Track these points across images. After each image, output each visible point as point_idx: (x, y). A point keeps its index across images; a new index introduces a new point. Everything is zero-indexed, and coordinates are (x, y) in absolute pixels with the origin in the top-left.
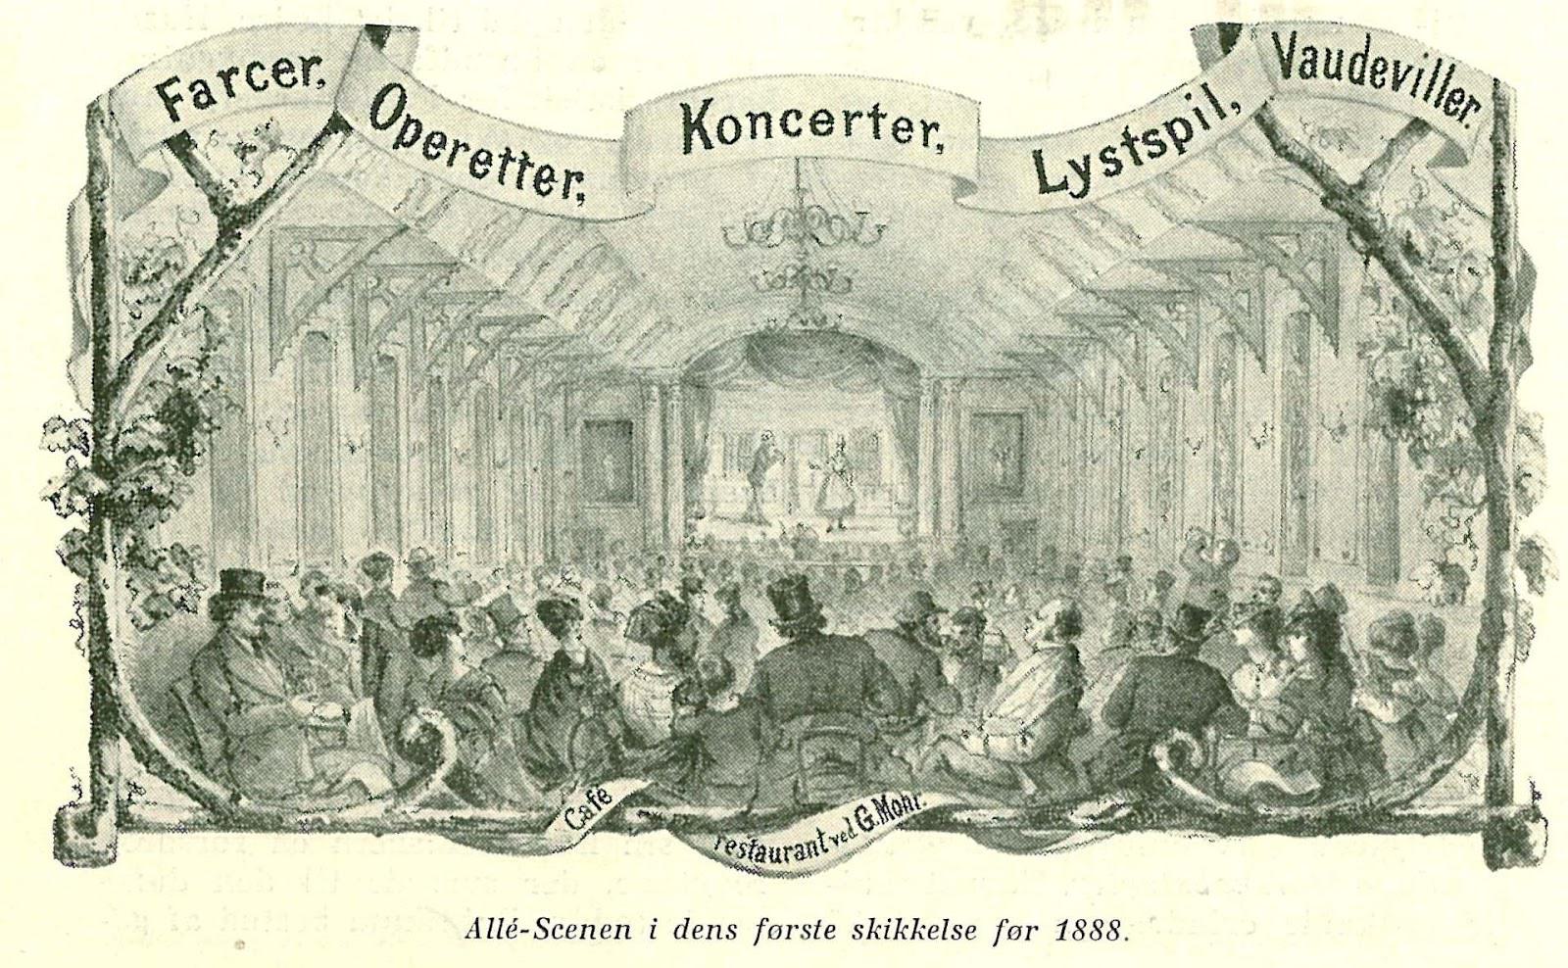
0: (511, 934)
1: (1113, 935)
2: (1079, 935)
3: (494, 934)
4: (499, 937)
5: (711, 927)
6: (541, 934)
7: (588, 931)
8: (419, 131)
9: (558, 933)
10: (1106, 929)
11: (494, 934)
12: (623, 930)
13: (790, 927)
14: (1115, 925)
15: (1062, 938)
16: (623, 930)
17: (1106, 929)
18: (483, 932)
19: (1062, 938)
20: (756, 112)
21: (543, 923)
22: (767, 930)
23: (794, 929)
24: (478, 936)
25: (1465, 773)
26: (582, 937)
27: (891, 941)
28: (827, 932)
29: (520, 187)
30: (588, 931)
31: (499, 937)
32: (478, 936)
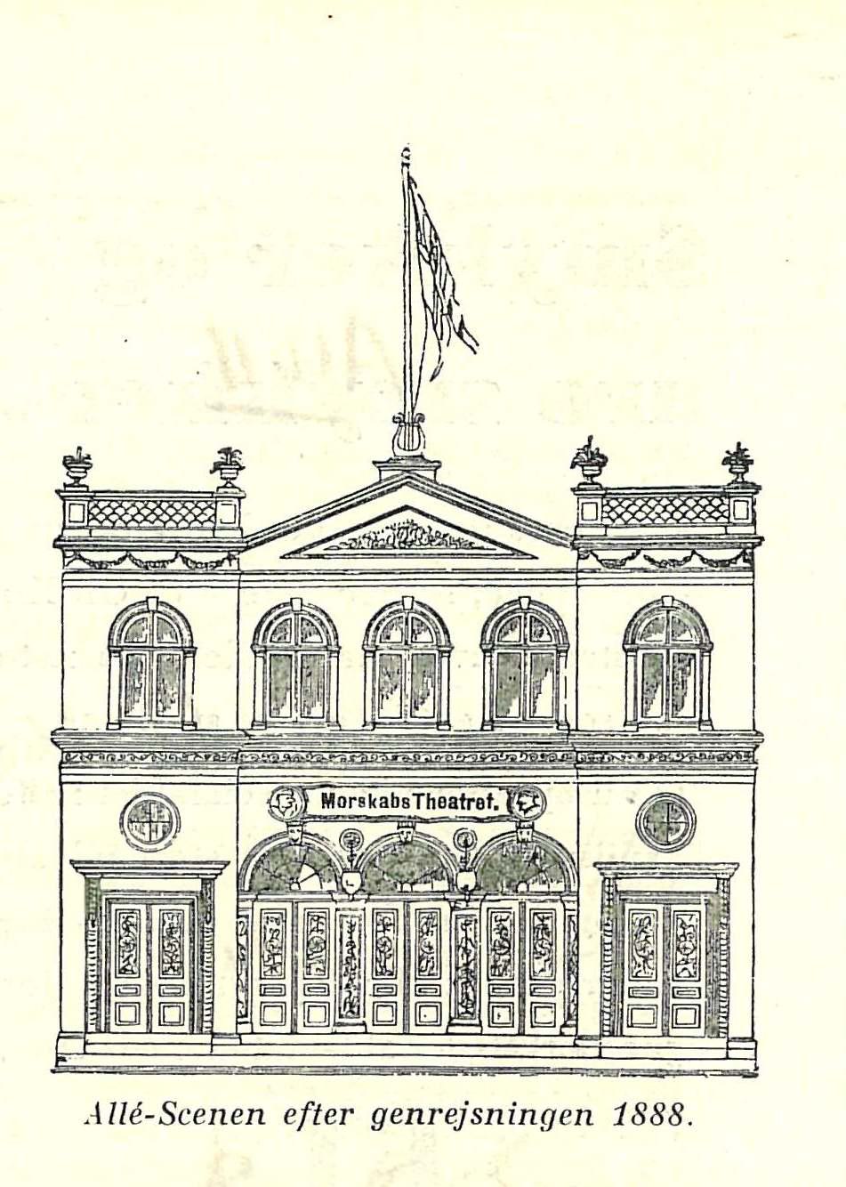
0: (135, 1120)
1: (675, 1120)
2: (638, 1119)
3: (116, 1118)
4: (122, 1123)
5: (580, 1112)
6: (167, 1119)
7: (218, 1115)
8: (339, 805)
9: (185, 1118)
10: (667, 1114)
11: (116, 1118)
12: (584, 1116)
13: (433, 1111)
14: (678, 1108)
15: (620, 1123)
16: (584, 1116)
17: (649, 1113)
18: (105, 1116)
19: (620, 1123)
20: (758, 771)
21: (170, 1107)
22: (171, 1114)
23: (437, 1113)
24: (99, 1122)
25: (349, 935)
26: (212, 1123)
27: (517, 1126)
28: (327, 1116)
29: (418, 808)
30: (218, 1115)
31: (122, 1123)
32: (99, 1122)
